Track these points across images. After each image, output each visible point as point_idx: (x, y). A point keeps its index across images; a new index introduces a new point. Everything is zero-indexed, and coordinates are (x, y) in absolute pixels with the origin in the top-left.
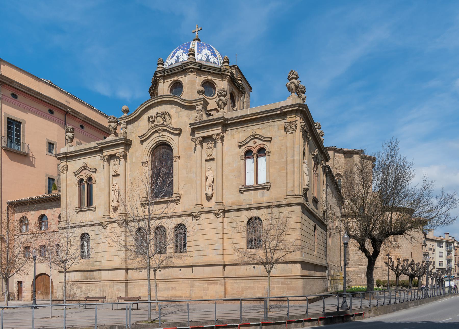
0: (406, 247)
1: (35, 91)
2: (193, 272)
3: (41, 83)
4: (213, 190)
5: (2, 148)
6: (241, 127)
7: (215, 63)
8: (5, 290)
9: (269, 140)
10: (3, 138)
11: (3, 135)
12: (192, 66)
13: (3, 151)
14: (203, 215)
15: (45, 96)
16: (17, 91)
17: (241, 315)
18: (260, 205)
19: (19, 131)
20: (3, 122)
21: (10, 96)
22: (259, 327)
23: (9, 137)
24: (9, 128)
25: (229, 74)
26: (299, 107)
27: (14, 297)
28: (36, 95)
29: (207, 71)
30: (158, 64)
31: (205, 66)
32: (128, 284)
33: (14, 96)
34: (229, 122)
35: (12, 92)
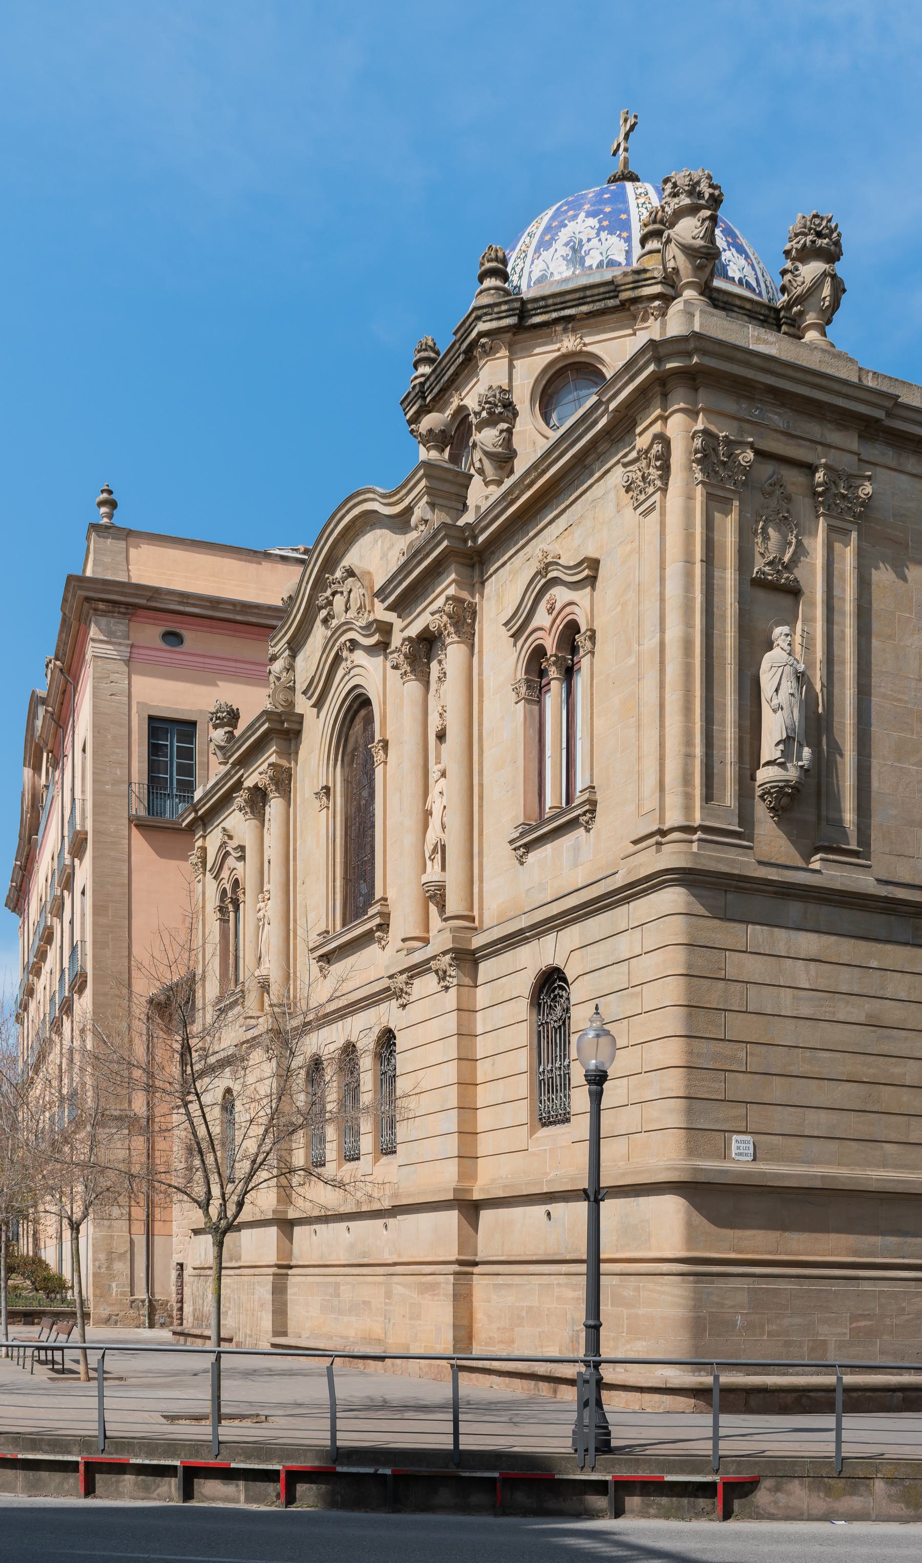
3: (266, 565)
4: (443, 868)
5: (130, 821)
6: (521, 543)
7: (612, 263)
8: (141, 1294)
9: (589, 573)
10: (135, 788)
11: (135, 778)
12: (482, 326)
13: (135, 831)
14: (416, 982)
16: (179, 618)
17: (103, 1422)
18: (555, 909)
20: (135, 736)
21: (159, 643)
23: (155, 783)
24: (155, 749)
25: (657, 289)
27: (171, 1316)
28: (241, 613)
29: (556, 321)
31: (543, 298)
32: (292, 1280)
34: (481, 539)
35: (161, 630)
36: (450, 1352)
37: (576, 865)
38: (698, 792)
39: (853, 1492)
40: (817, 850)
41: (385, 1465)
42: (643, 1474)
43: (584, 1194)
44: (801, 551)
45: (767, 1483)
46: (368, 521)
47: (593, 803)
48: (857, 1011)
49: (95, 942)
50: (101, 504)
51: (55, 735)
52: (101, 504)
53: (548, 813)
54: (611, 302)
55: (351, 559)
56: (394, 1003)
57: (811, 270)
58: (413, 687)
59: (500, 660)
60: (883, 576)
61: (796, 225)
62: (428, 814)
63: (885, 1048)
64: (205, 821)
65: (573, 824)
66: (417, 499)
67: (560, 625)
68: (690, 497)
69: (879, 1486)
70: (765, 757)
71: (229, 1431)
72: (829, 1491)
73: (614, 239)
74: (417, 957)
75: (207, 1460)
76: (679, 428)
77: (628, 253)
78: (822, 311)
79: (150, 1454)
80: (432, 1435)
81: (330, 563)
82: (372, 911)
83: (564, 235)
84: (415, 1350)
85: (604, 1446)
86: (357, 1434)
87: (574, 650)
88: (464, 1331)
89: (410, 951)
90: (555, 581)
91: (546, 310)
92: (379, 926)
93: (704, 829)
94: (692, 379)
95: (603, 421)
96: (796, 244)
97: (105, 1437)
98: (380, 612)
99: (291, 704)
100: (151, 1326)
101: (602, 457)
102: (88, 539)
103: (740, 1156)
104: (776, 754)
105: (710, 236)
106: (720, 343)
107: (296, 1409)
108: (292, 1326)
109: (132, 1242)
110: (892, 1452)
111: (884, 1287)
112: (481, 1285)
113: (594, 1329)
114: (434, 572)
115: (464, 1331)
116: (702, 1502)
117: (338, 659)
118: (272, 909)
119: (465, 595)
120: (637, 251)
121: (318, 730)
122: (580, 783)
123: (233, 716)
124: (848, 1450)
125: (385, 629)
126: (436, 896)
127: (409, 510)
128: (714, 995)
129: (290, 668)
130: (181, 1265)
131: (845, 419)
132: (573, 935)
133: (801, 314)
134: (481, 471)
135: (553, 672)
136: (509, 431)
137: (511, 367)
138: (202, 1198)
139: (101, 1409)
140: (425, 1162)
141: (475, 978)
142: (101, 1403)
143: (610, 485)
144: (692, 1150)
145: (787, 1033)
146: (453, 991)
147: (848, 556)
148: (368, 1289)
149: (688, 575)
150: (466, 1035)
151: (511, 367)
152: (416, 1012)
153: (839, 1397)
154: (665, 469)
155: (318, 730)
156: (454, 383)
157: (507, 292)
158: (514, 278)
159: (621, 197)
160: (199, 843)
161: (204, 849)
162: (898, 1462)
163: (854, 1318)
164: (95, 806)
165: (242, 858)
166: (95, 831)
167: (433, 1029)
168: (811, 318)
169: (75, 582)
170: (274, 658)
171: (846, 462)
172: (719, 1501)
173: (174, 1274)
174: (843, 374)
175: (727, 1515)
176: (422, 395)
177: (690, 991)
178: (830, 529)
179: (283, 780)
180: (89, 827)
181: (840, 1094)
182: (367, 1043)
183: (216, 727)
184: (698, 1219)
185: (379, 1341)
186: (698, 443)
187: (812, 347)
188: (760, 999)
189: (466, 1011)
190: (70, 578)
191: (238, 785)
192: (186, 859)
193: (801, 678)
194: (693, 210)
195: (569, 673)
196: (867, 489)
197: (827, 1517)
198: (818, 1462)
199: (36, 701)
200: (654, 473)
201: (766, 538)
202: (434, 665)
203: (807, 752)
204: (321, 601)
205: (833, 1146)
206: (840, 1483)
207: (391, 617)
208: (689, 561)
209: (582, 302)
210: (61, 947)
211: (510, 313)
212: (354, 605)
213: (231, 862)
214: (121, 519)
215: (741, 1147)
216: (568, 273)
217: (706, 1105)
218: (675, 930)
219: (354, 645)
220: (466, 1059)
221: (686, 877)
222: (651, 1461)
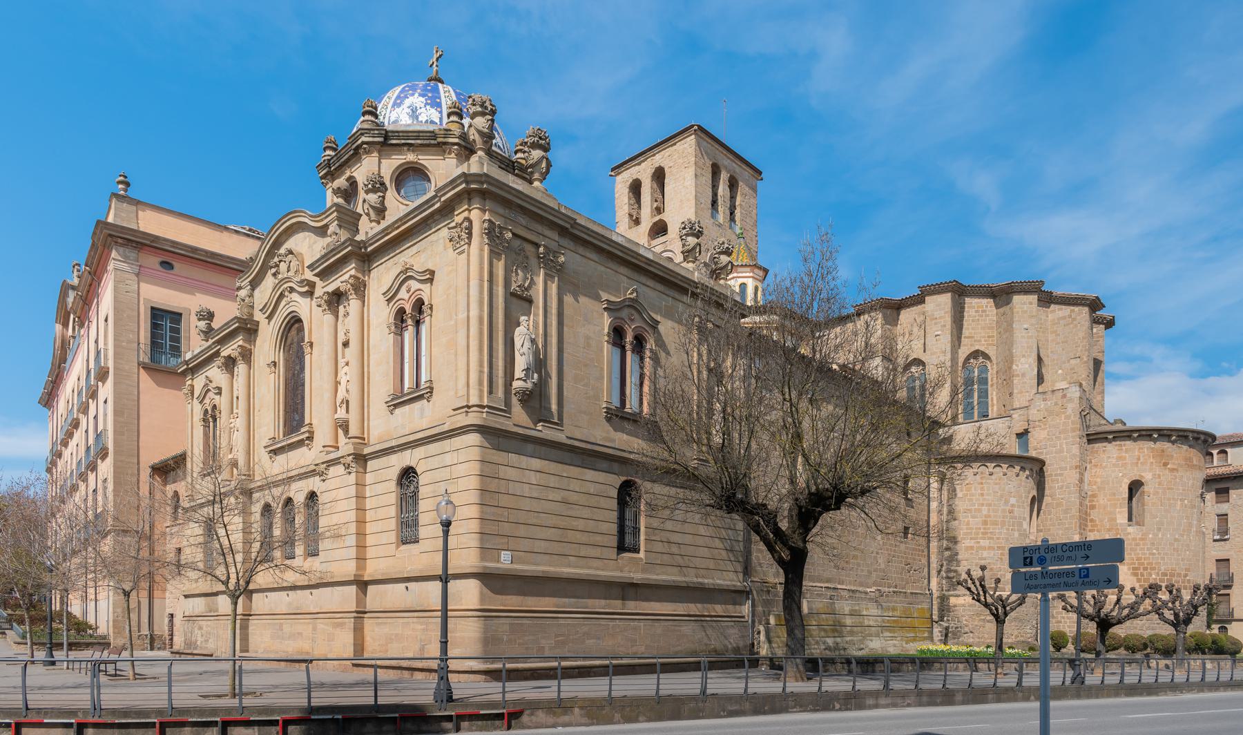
0: (1176, 540)
1: (206, 252)
2: (186, 596)
3: (226, 234)
4: (347, 411)
7: (432, 122)
9: (430, 277)
11: (142, 340)
12: (364, 139)
14: (331, 468)
15: (228, 257)
17: (170, 699)
18: (412, 438)
19: (178, 331)
20: (142, 317)
22: (274, 730)
23: (155, 344)
24: (155, 326)
25: (456, 140)
26: (467, 183)
30: (325, 149)
32: (251, 622)
33: (167, 265)
36: (352, 656)
37: (422, 418)
38: (486, 389)
39: (565, 713)
40: (540, 421)
41: (338, 713)
42: (470, 711)
43: (439, 578)
44: (532, 282)
45: (527, 712)
46: (300, 227)
47: (432, 388)
48: (556, 496)
49: (115, 431)
50: (119, 182)
51: (82, 308)
52: (119, 182)
53: (406, 390)
54: (433, 142)
55: (291, 244)
56: (317, 478)
57: (537, 154)
58: (329, 317)
59: (380, 314)
60: (568, 299)
61: (530, 131)
62: (337, 383)
63: (569, 513)
64: (194, 370)
65: (421, 397)
66: (332, 221)
67: (413, 299)
68: (482, 250)
69: (577, 710)
70: (517, 375)
71: (247, 701)
72: (555, 714)
73: (433, 110)
74: (332, 456)
75: (236, 716)
76: (477, 216)
77: (441, 119)
78: (542, 174)
79: (201, 715)
80: (364, 698)
81: (277, 244)
82: (303, 430)
83: (407, 102)
84: (329, 656)
85: (450, 699)
86: (320, 699)
87: (420, 312)
88: (359, 646)
89: (328, 453)
90: (411, 278)
91: (398, 138)
92: (308, 438)
93: (489, 407)
94: (483, 194)
95: (438, 205)
96: (530, 140)
97: (27, 709)
98: (309, 275)
99: (252, 315)
100: (152, 649)
101: (437, 222)
102: (110, 200)
103: (505, 561)
104: (522, 375)
105: (491, 127)
106: (497, 181)
107: (288, 689)
108: (252, 647)
109: (139, 602)
110: (580, 695)
111: (569, 621)
112: (368, 623)
113: (444, 644)
114: (343, 261)
115: (359, 646)
116: (497, 722)
117: (282, 296)
118: (240, 423)
119: (360, 275)
120: (445, 120)
121: (268, 333)
122: (424, 378)
123: (210, 316)
124: (563, 695)
125: (312, 285)
126: (344, 426)
127: (326, 226)
128: (493, 486)
129: (251, 296)
130: (172, 615)
131: (553, 225)
132: (420, 452)
133: (532, 173)
134: (368, 214)
135: (410, 322)
136: (384, 197)
137: (380, 163)
138: (224, 578)
139: (170, 692)
140: (336, 558)
141: (365, 468)
142: (170, 690)
143: (440, 236)
144: (483, 558)
145: (526, 504)
146: (353, 475)
147: (554, 288)
148: (304, 626)
149: (481, 286)
150: (360, 497)
151: (380, 163)
152: (330, 484)
153: (559, 671)
154: (470, 234)
155: (268, 333)
156: (347, 164)
157: (378, 125)
158: (381, 118)
159: (436, 90)
160: (189, 382)
161: (192, 386)
162: (584, 699)
163: (557, 636)
164: (116, 354)
165: (220, 393)
166: (115, 368)
167: (342, 493)
168: (536, 176)
169: (101, 225)
170: (240, 288)
171: (553, 245)
172: (505, 722)
173: (167, 620)
174: (551, 205)
175: (509, 728)
176: (329, 166)
177: (482, 482)
178: (546, 274)
179: (247, 356)
180: (111, 364)
181: (551, 533)
182: (300, 498)
183: (199, 320)
184: (486, 590)
185: (308, 653)
186: (486, 225)
187: (536, 189)
188: (513, 488)
189: (360, 485)
190: (98, 222)
191: (217, 354)
192: (181, 390)
193: (533, 341)
194: (483, 114)
195: (418, 323)
196: (562, 259)
197: (554, 726)
198: (550, 701)
199: (66, 288)
200: (464, 236)
201: (517, 274)
202: (341, 308)
203: (536, 376)
204: (272, 263)
205: (547, 557)
206: (560, 710)
207: (316, 279)
208: (481, 280)
209: (417, 138)
210: (87, 431)
211: (379, 135)
212: (293, 269)
213: (211, 395)
214: (131, 193)
215: (505, 556)
216: (409, 122)
217: (489, 540)
218: (475, 453)
219: (292, 290)
220: (361, 509)
221: (481, 429)
222: (472, 705)
